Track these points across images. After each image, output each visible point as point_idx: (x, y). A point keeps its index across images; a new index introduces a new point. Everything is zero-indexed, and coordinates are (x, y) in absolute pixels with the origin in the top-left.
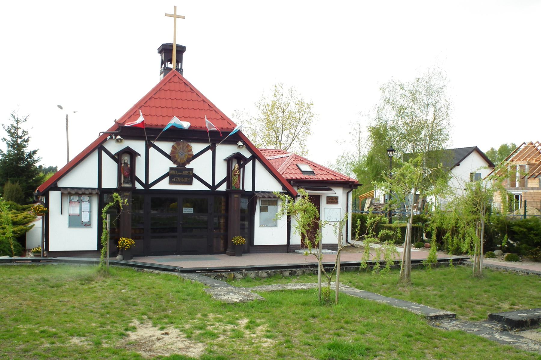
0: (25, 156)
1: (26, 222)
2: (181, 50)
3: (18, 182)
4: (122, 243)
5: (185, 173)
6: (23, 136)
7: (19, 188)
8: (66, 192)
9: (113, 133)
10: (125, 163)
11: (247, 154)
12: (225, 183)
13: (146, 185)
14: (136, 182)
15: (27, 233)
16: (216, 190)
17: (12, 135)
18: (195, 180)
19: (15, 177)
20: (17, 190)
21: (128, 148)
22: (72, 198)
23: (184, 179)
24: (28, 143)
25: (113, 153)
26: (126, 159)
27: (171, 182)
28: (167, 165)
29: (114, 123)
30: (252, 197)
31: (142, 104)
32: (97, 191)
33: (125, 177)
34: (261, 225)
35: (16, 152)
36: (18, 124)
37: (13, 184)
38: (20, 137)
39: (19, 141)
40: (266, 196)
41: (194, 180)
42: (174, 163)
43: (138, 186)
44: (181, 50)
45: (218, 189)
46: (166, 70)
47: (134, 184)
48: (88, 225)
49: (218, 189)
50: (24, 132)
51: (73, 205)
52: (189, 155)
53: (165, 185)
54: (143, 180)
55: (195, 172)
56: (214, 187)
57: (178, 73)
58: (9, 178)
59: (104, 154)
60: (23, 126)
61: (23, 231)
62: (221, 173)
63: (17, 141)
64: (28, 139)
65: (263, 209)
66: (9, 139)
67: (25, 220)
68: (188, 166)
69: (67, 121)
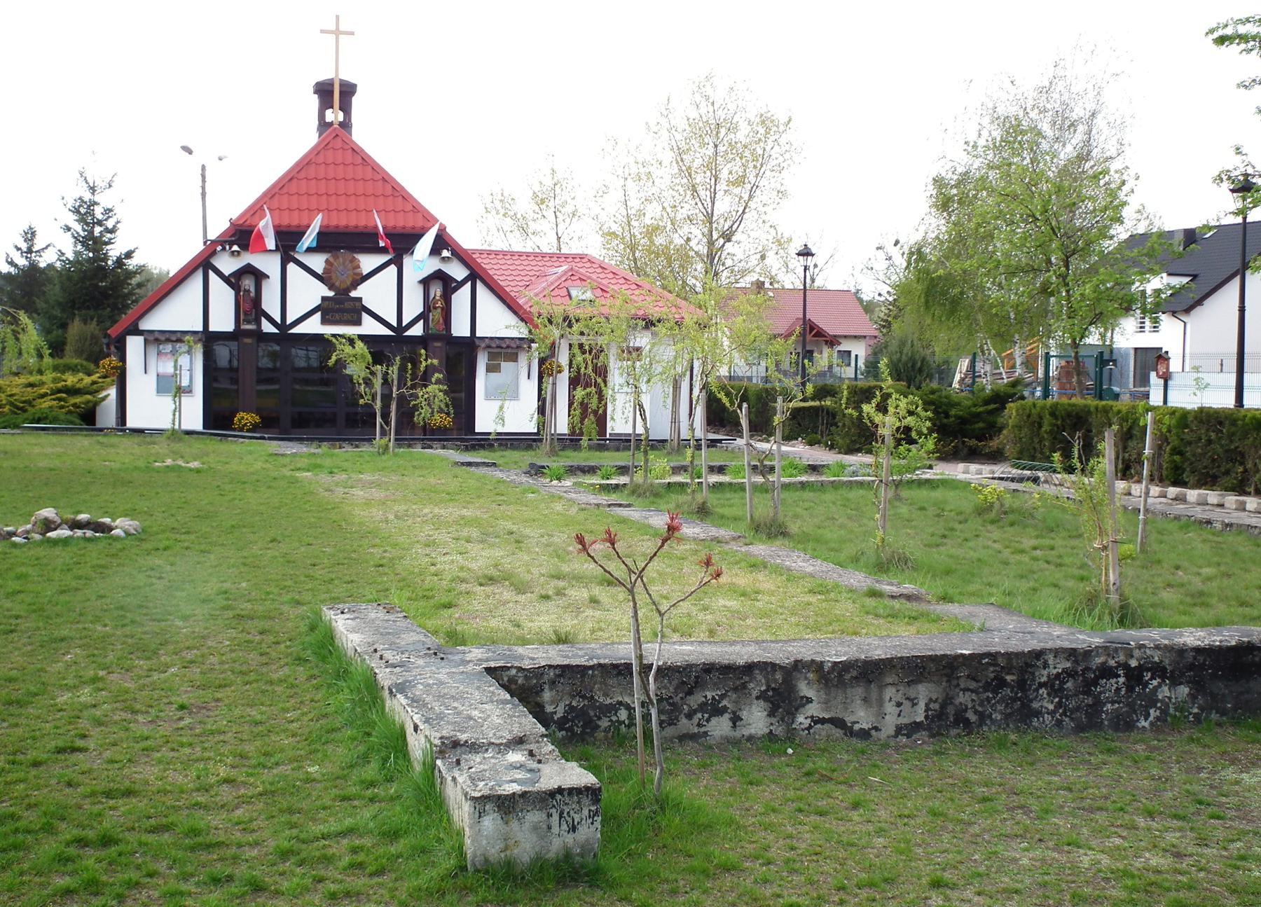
0: (110, 263)
1: (94, 390)
2: (349, 90)
4: (240, 421)
5: (348, 305)
6: (106, 220)
7: (97, 332)
8: (151, 338)
9: (225, 242)
10: (245, 290)
11: (457, 272)
13: (283, 326)
14: (263, 319)
15: (98, 409)
16: (405, 334)
17: (82, 220)
18: (366, 318)
19: (88, 308)
20: (93, 337)
21: (249, 265)
22: (161, 347)
23: (347, 316)
24: (117, 233)
25: (227, 273)
26: (248, 283)
27: (324, 321)
28: (315, 291)
29: (228, 225)
30: (470, 345)
32: (200, 335)
33: (246, 314)
34: (488, 397)
35: (91, 255)
36: (93, 194)
37: (85, 324)
38: (100, 223)
39: (97, 230)
40: (494, 345)
41: (365, 317)
42: (330, 289)
43: (267, 327)
44: (348, 91)
45: (408, 333)
46: (323, 125)
47: (259, 324)
49: (408, 333)
50: (108, 211)
51: (163, 358)
52: (355, 274)
53: (313, 326)
54: (278, 318)
55: (365, 303)
56: (400, 329)
58: (76, 312)
59: (212, 274)
60: (104, 200)
61: (91, 405)
62: (414, 306)
63: (92, 232)
64: (114, 226)
65: (491, 369)
66: (78, 227)
67: (95, 387)
68: (353, 294)
69: (203, 188)
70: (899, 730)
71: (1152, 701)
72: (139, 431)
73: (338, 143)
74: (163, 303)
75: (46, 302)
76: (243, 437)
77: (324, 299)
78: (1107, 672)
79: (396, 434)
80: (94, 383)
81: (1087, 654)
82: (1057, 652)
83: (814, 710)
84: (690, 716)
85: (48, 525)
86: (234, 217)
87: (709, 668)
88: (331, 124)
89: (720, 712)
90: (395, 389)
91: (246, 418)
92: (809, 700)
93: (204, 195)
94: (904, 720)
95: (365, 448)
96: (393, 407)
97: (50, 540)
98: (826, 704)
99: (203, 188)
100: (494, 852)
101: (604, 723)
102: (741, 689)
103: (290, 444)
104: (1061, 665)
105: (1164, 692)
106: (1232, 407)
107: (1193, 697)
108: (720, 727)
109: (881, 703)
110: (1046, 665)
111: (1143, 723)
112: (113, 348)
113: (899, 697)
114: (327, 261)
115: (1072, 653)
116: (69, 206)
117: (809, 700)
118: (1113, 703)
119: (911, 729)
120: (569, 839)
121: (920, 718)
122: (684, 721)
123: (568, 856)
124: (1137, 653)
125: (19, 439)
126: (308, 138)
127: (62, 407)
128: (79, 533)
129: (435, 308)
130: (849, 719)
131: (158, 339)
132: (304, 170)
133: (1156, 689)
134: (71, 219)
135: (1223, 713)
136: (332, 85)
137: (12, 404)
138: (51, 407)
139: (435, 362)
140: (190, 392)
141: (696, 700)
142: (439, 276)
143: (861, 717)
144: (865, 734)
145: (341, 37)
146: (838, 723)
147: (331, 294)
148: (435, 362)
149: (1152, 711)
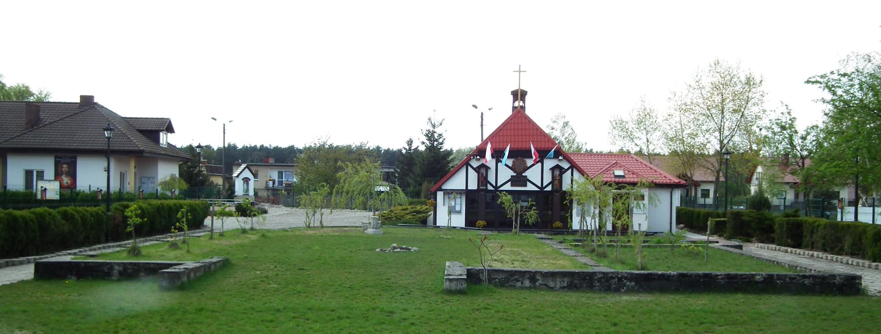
3: (433, 182)
4: (478, 224)
11: (566, 165)
12: (551, 185)
15: (428, 219)
17: (429, 139)
18: (529, 183)
27: (512, 185)
31: (494, 134)
33: (481, 182)
36: (434, 128)
38: (436, 140)
39: (436, 143)
42: (514, 172)
43: (490, 188)
47: (487, 186)
48: (459, 212)
50: (440, 135)
56: (542, 188)
57: (521, 110)
59: (469, 167)
60: (438, 130)
61: (425, 217)
62: (548, 179)
64: (443, 141)
66: (428, 142)
68: (524, 174)
69: (482, 123)
70: (560, 288)
71: (625, 285)
72: (439, 227)
73: (519, 115)
74: (456, 174)
75: (414, 175)
76: (473, 229)
77: (512, 176)
78: (612, 278)
79: (520, 228)
80: (426, 209)
81: (607, 273)
82: (599, 273)
83: (540, 282)
84: (512, 281)
85: (395, 248)
86: (478, 145)
87: (516, 271)
88: (517, 107)
89: (519, 281)
90: (519, 212)
91: (481, 223)
92: (539, 280)
93: (482, 125)
94: (561, 286)
95: (509, 233)
96: (519, 218)
97: (395, 251)
98: (543, 281)
99: (482, 123)
100: (448, 288)
101: (493, 282)
102: (523, 276)
103: (484, 231)
104: (601, 276)
105: (628, 283)
106: (853, 220)
107: (636, 285)
108: (519, 284)
109: (556, 281)
110: (597, 275)
111: (622, 290)
112: (432, 196)
113: (560, 280)
114: (513, 162)
115: (603, 273)
116: (424, 134)
117: (539, 280)
118: (614, 285)
119: (563, 288)
120: (461, 287)
121: (565, 285)
122: (511, 282)
123: (461, 289)
124: (620, 274)
125: (397, 229)
126: (509, 113)
127: (414, 218)
128: (402, 250)
129: (556, 180)
130: (548, 284)
131: (448, 193)
132: (505, 126)
133: (626, 283)
134: (424, 139)
135: (644, 289)
136: (518, 92)
137: (396, 217)
138: (410, 218)
139: (534, 203)
140: (460, 213)
141: (513, 278)
142: (557, 167)
143: (551, 284)
144: (552, 288)
145: (518, 73)
146: (546, 285)
147: (515, 174)
148: (534, 203)
149: (625, 288)
